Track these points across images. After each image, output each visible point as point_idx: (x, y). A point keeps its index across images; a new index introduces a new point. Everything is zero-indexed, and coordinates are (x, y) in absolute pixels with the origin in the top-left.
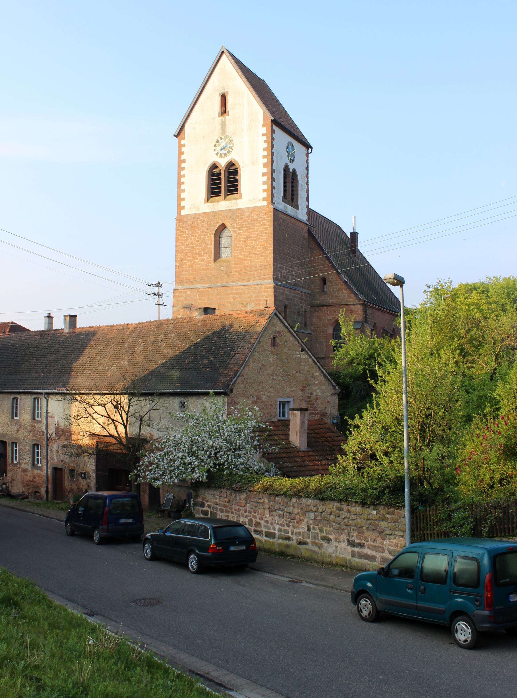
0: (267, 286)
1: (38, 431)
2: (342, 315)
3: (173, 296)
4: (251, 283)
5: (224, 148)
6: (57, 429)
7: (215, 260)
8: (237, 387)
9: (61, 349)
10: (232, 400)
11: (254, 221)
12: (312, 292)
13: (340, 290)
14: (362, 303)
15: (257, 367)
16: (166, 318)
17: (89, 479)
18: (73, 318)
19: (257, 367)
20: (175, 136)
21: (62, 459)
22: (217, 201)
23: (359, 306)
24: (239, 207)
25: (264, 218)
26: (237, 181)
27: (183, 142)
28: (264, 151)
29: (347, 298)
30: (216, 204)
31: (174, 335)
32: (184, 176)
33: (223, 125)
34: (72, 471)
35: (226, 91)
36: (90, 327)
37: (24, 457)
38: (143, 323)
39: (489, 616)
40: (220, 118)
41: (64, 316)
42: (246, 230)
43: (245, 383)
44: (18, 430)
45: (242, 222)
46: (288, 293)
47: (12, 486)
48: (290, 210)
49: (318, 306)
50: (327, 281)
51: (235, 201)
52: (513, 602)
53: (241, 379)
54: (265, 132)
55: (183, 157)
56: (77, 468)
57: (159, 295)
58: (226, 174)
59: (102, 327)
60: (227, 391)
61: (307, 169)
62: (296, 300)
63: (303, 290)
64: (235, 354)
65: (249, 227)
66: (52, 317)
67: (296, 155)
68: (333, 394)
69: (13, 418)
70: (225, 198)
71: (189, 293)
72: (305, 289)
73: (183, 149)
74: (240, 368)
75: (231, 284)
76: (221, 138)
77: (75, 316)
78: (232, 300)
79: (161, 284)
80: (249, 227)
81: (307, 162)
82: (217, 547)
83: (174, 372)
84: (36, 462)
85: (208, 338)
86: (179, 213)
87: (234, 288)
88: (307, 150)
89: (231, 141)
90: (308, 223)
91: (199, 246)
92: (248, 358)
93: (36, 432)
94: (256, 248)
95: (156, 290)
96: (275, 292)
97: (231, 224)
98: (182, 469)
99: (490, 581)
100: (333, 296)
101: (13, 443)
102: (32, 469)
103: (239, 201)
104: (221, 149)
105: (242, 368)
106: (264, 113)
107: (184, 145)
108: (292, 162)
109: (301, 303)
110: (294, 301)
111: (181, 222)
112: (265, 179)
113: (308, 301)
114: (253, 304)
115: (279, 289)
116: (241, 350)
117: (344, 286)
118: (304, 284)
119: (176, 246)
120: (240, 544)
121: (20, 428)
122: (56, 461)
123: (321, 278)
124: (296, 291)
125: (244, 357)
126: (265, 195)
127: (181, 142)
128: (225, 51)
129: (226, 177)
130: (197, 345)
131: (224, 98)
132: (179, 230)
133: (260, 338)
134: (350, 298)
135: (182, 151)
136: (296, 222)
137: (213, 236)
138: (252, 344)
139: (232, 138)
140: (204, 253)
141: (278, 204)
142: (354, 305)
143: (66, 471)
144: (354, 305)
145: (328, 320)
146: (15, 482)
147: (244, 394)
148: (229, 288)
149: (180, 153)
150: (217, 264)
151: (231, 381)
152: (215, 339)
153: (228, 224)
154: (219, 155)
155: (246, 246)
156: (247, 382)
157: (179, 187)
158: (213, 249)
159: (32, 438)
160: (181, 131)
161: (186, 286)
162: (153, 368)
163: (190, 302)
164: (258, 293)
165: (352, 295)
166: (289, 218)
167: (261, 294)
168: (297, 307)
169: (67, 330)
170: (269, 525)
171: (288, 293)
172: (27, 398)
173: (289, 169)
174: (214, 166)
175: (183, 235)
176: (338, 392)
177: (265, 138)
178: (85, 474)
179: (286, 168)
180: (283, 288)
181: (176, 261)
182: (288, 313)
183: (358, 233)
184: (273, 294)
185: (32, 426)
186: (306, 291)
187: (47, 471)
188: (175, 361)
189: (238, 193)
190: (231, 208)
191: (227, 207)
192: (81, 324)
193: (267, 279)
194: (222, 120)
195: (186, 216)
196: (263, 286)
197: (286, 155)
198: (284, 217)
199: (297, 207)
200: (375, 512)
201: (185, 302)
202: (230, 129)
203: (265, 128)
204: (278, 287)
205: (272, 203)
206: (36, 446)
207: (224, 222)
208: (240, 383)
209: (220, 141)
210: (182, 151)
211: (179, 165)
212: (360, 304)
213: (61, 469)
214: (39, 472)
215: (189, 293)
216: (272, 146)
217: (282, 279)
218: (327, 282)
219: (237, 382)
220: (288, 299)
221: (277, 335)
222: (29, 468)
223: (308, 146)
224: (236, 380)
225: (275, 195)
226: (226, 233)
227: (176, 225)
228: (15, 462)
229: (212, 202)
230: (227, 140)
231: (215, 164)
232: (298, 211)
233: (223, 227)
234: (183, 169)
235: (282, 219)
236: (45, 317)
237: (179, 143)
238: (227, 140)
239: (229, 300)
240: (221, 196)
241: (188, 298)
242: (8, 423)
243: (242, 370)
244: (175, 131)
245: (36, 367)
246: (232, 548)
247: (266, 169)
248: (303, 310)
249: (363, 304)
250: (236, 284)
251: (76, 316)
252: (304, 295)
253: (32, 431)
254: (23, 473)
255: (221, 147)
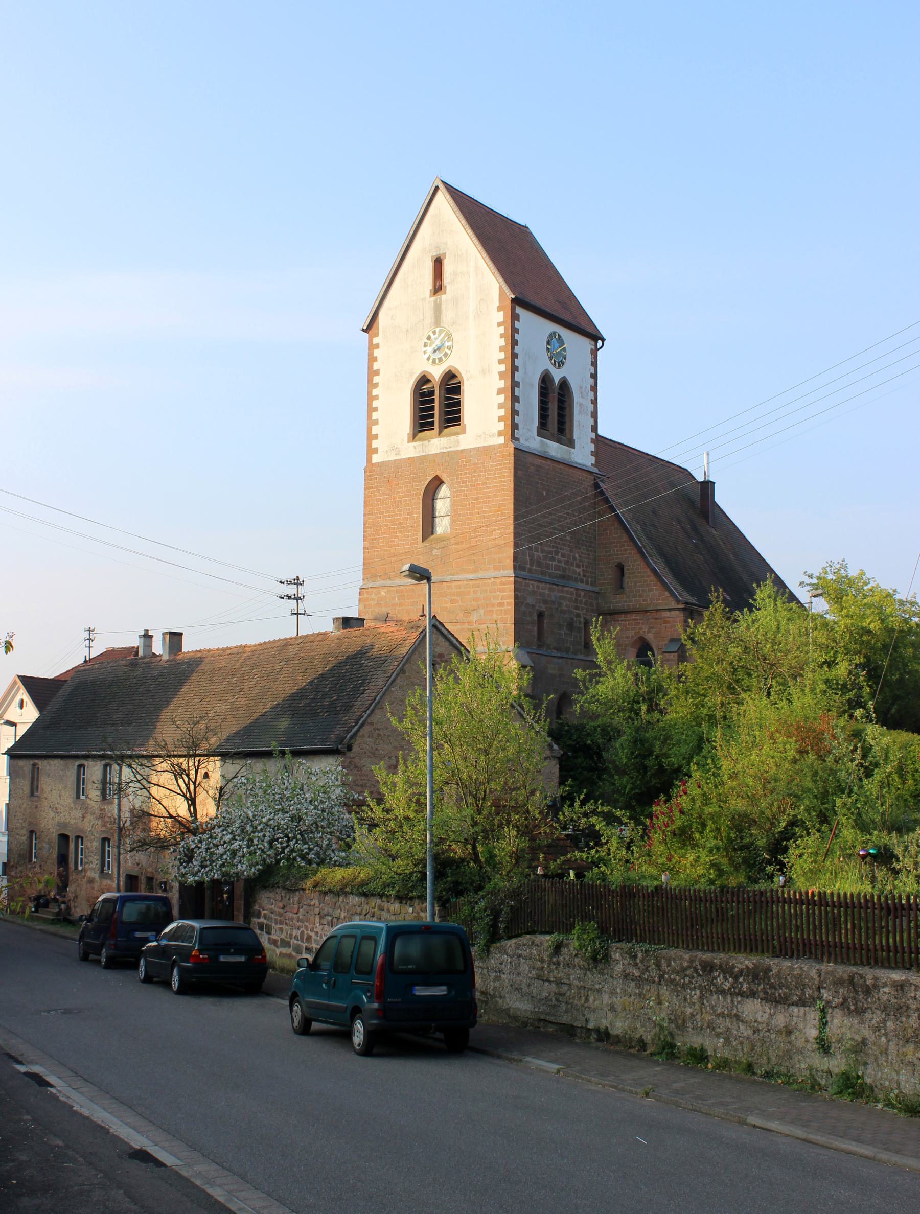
0: (504, 579)
1: (109, 817)
2: (596, 627)
3: (360, 600)
4: (479, 575)
5: (439, 349)
6: (132, 811)
7: (424, 539)
8: (359, 742)
9: (152, 687)
10: (350, 763)
11: (485, 471)
12: (601, 589)
13: (647, 586)
14: (683, 606)
15: (398, 710)
16: (305, 634)
17: (171, 892)
18: (176, 638)
19: (398, 710)
20: (363, 330)
21: (137, 861)
22: (428, 439)
23: (677, 613)
24: (462, 447)
25: (500, 465)
26: (458, 403)
27: (376, 341)
28: (500, 351)
29: (659, 599)
30: (426, 442)
31: (297, 662)
32: (376, 397)
33: (438, 311)
34: (150, 880)
35: (441, 252)
36: (197, 651)
37: (91, 859)
38: (265, 643)
39: (377, 1010)
40: (433, 299)
41: (163, 634)
42: (472, 486)
43: (375, 735)
44: (83, 817)
45: (466, 473)
46: (547, 592)
47: (75, 907)
48: (554, 449)
49: (611, 614)
50: (625, 568)
51: (455, 437)
52: (419, 996)
53: (366, 730)
54: (501, 319)
55: (376, 366)
56: (156, 876)
57: (297, 599)
58: (443, 392)
59: (212, 651)
60: (340, 747)
61: (594, 376)
62: (565, 604)
63: (580, 586)
64: (365, 690)
65: (476, 481)
66: (152, 636)
67: (568, 354)
68: (549, 757)
69: (78, 797)
70: (440, 433)
71: (383, 593)
72: (587, 583)
73: (376, 353)
74: (366, 712)
75: (448, 578)
76: (434, 333)
77: (180, 634)
78: (449, 605)
79: (301, 580)
80: (476, 481)
81: (594, 364)
82: (200, 954)
83: (284, 719)
84: (106, 868)
85: (339, 666)
86: (369, 459)
87: (453, 584)
88: (593, 343)
89: (449, 337)
90: (595, 470)
91: (400, 515)
92: (381, 697)
93: (107, 819)
94: (488, 517)
95: (292, 590)
96: (516, 590)
97: (448, 476)
98: (226, 859)
99: (383, 965)
100: (635, 596)
101: (78, 837)
102: (101, 878)
103: (461, 437)
104: (435, 351)
105: (368, 712)
106: (500, 288)
107: (377, 346)
108: (559, 366)
109: (577, 608)
110: (560, 604)
111: (373, 475)
112: (501, 398)
113: (592, 605)
114: (482, 611)
115: (527, 585)
116: (373, 684)
117: (653, 578)
118: (584, 576)
119: (365, 515)
120: (238, 952)
121: (86, 813)
122: (130, 864)
123: (616, 564)
124: (566, 589)
125: (374, 694)
126: (501, 426)
127: (372, 340)
128: (441, 186)
129: (443, 398)
130: (322, 677)
131: (438, 263)
132: (369, 488)
133: (404, 665)
134: (663, 599)
135: (375, 355)
136: (567, 469)
137: (421, 497)
138: (389, 675)
139: (451, 331)
140: (407, 527)
141: (527, 440)
142: (670, 610)
143: (143, 880)
144: (670, 610)
145: (627, 637)
146: (79, 900)
147: (374, 754)
148: (444, 584)
149: (372, 359)
150: (427, 543)
151: (348, 732)
152: (347, 667)
153: (444, 477)
154: (431, 360)
155: (472, 514)
156: (379, 735)
157: (369, 417)
158: (421, 520)
159: (100, 829)
160: (374, 321)
161: (380, 583)
162: (260, 714)
163: (384, 610)
164: (491, 592)
165: (667, 594)
166: (549, 462)
167: (494, 594)
168: (567, 616)
169: (166, 657)
170: (318, 938)
171: (547, 592)
172: (96, 765)
173: (552, 380)
174: (424, 380)
175: (375, 496)
176: (559, 755)
177: (502, 330)
178: (165, 883)
179: (546, 379)
180: (535, 584)
181: (364, 541)
182: (545, 625)
183: (714, 483)
184: (512, 594)
185: (101, 810)
186: (589, 587)
187: (119, 880)
188: (289, 702)
189: (459, 425)
190: (448, 450)
191: (443, 448)
192: (188, 646)
193: (504, 568)
194: (435, 302)
195: (381, 465)
196: (498, 581)
197: (545, 356)
198: (538, 461)
199: (571, 443)
200: (411, 910)
201: (377, 610)
202: (448, 315)
203: (502, 313)
204: (524, 581)
205: (513, 438)
206: (105, 840)
207: (438, 473)
208: (367, 735)
209: (433, 337)
210: (375, 355)
211: (370, 380)
212: (678, 609)
213: (136, 877)
214: (109, 882)
215: (383, 593)
216: (514, 343)
217: (534, 567)
218: (626, 571)
219: (360, 733)
220: (545, 602)
221: (438, 660)
222: (96, 876)
223: (595, 337)
224: (358, 730)
225: (520, 426)
226: (444, 491)
227: (365, 480)
228: (80, 868)
229: (420, 440)
230: (442, 335)
231: (424, 376)
232: (572, 450)
233: (437, 482)
234: (376, 385)
235: (533, 465)
236: (140, 636)
237: (370, 341)
238: (442, 335)
239: (445, 605)
240: (433, 429)
241: (382, 603)
242: (72, 805)
243: (369, 715)
244: (364, 322)
245: (115, 717)
246: (222, 958)
247: (503, 381)
248: (582, 620)
249: (683, 609)
250: (455, 578)
251: (181, 634)
252: (582, 594)
253: (101, 817)
254: (89, 886)
255: (434, 346)
